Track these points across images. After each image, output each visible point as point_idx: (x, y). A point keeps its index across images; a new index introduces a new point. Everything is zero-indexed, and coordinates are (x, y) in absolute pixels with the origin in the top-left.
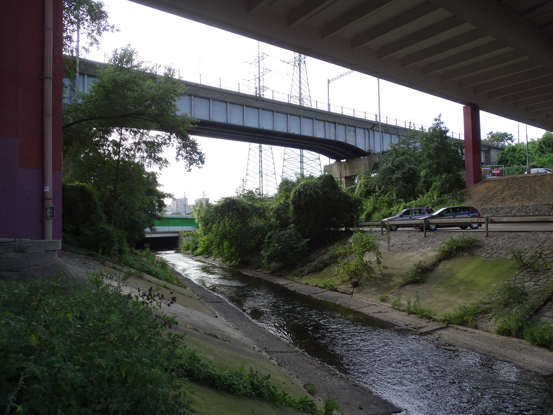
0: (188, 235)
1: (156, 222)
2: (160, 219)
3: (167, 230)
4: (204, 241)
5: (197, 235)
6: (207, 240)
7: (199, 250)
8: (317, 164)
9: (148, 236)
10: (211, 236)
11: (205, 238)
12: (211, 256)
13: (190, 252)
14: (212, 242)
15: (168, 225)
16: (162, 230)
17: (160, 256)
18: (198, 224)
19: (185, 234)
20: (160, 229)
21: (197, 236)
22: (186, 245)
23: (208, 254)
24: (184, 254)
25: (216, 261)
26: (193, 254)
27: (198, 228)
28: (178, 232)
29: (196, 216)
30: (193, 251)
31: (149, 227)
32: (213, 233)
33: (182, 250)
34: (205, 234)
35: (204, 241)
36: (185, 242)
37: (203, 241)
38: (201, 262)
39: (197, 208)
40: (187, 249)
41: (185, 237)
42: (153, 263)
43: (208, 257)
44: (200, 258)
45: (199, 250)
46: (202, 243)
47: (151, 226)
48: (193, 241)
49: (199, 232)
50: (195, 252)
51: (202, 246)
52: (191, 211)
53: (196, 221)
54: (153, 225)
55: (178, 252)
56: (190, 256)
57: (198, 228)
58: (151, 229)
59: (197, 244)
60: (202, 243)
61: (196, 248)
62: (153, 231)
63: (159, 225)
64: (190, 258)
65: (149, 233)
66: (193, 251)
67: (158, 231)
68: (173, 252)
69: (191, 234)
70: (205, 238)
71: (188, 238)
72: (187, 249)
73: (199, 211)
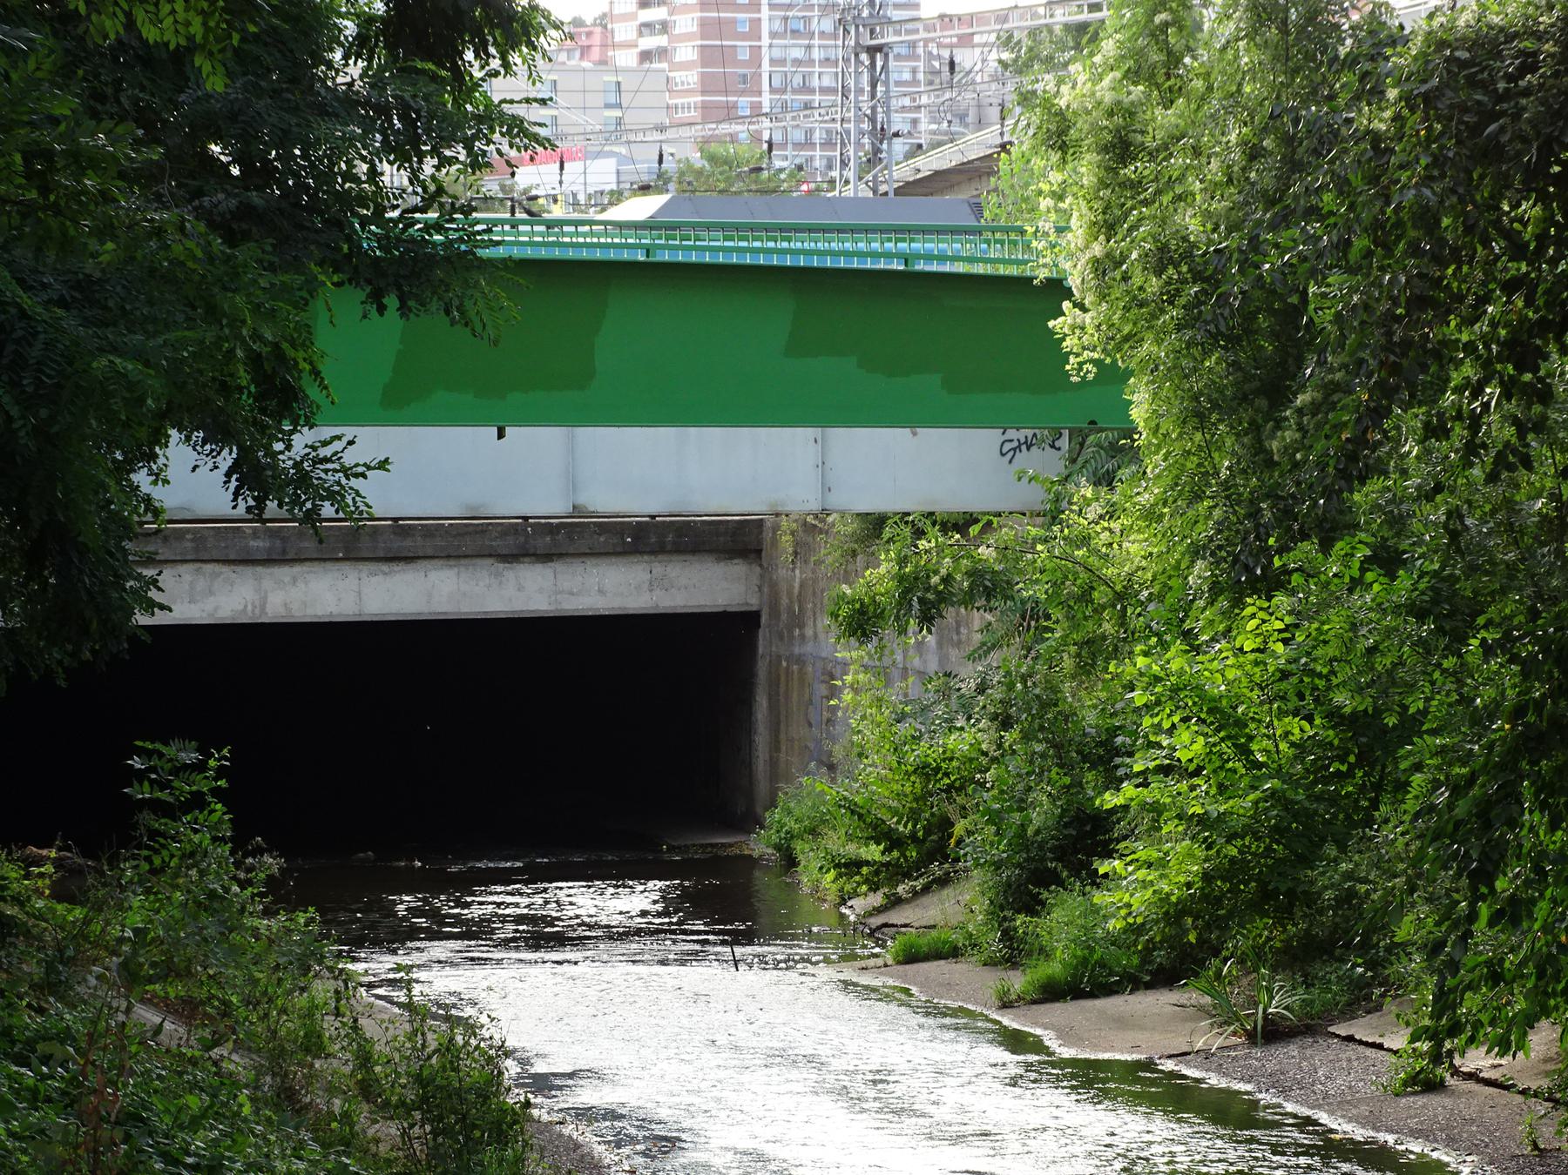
0: (925, 601)
1: (349, 334)
2: (427, 275)
3: (544, 501)
4: (1222, 718)
5: (1083, 593)
6: (1297, 688)
7: (1135, 887)
8: (1331, 1029)
9: (197, 598)
10: (1346, 605)
11: (1241, 651)
12: (1360, 1000)
13: (959, 906)
14: (1371, 741)
15: (565, 388)
16: (463, 495)
17: (441, 974)
18: (1112, 377)
19: (879, 575)
20: (419, 465)
21: (1098, 618)
22: (877, 781)
23: (1298, 959)
24: (851, 942)
25: (1466, 1101)
26: (1014, 953)
27: (1105, 452)
28: (737, 540)
29: (1059, 233)
30: (1025, 890)
31: (218, 432)
32: (1387, 560)
33: (815, 875)
34: (1247, 576)
35: (1222, 718)
36: (869, 719)
37: (1208, 696)
38: (1177, 1098)
39: (1085, 86)
40: (917, 850)
41: (862, 622)
42: (287, 1100)
43: (1305, 1028)
44: (1151, 1025)
45: (1135, 887)
46: (1189, 745)
47: (253, 403)
48: (1032, 715)
49: (1131, 535)
50: (1061, 925)
51: (1199, 799)
52: (975, 145)
53: (1078, 330)
54: (284, 398)
55: (728, 905)
56: (971, 981)
57: (1105, 452)
58: (252, 476)
59: (1106, 756)
60: (1189, 745)
61: (1085, 841)
62: (297, 512)
63: (401, 401)
64: (961, 1019)
65: (211, 546)
66: (1025, 890)
67: (384, 497)
68: (636, 901)
69: (988, 587)
70: (1241, 651)
71: (918, 648)
72: (917, 850)
73: (1121, 148)
